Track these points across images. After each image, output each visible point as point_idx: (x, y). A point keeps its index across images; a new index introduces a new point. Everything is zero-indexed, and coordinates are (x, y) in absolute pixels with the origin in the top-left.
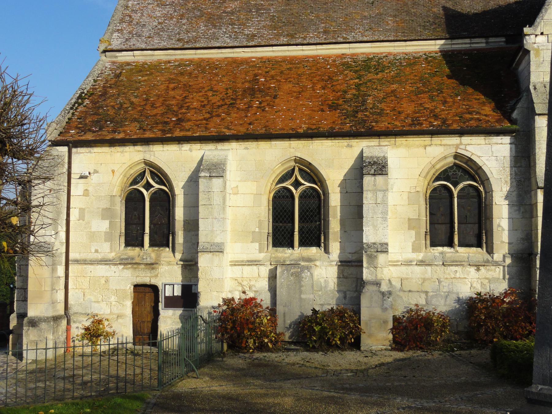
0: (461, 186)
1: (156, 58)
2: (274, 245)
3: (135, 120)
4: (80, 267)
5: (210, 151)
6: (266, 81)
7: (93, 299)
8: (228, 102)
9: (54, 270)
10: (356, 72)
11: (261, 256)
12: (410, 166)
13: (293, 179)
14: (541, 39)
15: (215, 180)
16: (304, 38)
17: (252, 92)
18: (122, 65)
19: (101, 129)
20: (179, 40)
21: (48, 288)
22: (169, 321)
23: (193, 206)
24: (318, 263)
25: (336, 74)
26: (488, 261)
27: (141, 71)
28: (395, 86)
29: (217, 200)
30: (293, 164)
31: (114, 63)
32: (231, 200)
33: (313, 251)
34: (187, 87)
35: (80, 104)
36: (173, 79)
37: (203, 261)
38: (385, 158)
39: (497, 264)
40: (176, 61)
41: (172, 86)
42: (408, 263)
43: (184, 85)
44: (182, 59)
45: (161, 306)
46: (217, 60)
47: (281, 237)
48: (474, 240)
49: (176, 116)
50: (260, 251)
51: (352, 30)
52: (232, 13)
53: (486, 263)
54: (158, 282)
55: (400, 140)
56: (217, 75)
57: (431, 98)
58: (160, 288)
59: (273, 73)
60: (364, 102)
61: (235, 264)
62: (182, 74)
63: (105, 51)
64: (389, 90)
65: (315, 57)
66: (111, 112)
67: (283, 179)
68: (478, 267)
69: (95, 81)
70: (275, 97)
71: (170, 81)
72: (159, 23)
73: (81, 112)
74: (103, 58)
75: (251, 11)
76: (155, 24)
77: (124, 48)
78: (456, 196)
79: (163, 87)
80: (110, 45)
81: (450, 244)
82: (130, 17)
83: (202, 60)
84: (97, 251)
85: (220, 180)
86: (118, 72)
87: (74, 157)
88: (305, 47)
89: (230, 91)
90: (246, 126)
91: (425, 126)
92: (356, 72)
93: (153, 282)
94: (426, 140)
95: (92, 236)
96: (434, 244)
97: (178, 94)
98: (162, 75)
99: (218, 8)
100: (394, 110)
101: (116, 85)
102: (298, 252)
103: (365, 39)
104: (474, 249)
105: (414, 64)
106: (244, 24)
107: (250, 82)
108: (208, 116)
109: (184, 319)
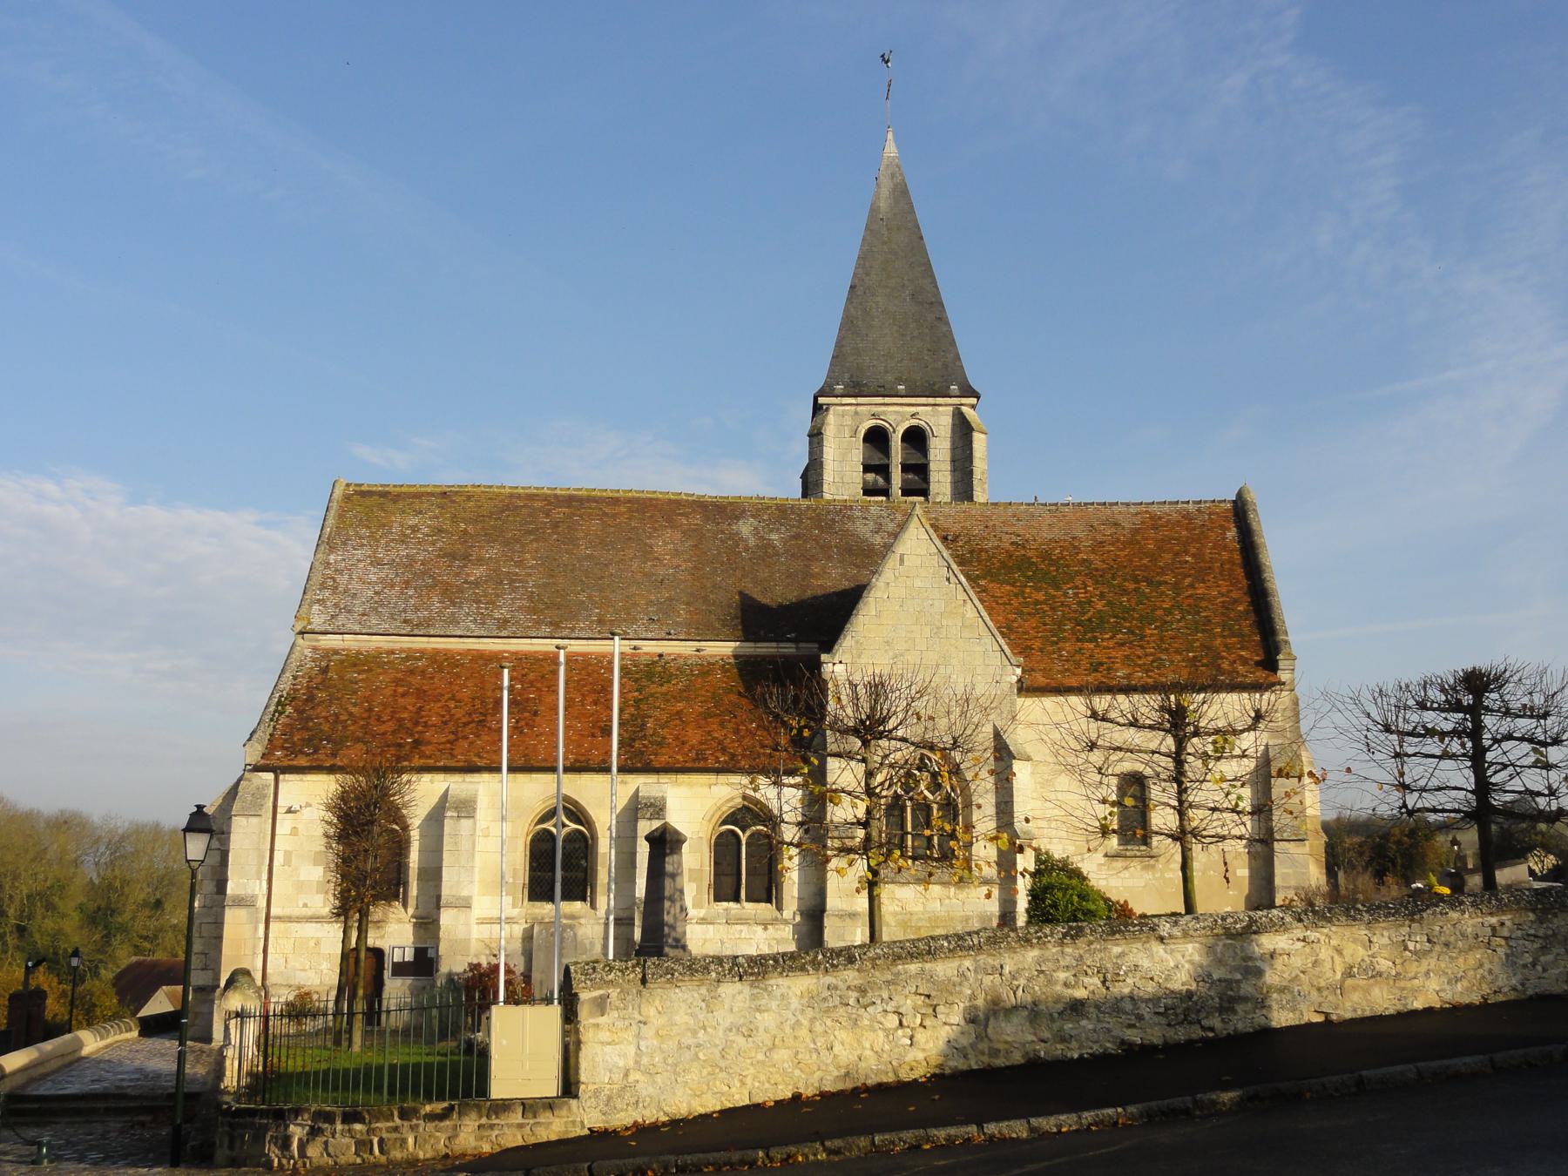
0: (748, 833)
1: (373, 645)
2: (530, 899)
3: (358, 740)
4: (282, 926)
5: (457, 784)
6: (523, 689)
7: (298, 966)
8: (476, 717)
10: (636, 681)
11: (515, 912)
12: (695, 805)
14: (839, 668)
15: (463, 821)
16: (573, 629)
18: (329, 653)
19: (316, 752)
20: (405, 621)
22: (396, 990)
23: (434, 850)
28: (680, 706)
29: (465, 845)
31: (315, 649)
32: (481, 844)
33: (577, 906)
34: (420, 693)
35: (281, 713)
37: (446, 918)
38: (664, 799)
39: (786, 922)
40: (402, 651)
41: (401, 690)
45: (387, 974)
47: (539, 889)
48: (764, 896)
49: (412, 735)
50: (514, 906)
51: (634, 621)
52: (477, 584)
53: (774, 921)
55: (682, 778)
56: (458, 676)
57: (722, 725)
59: (531, 676)
60: (643, 727)
61: (482, 922)
62: (412, 672)
63: (302, 633)
64: (675, 709)
66: (326, 727)
67: (543, 820)
68: (765, 926)
69: (295, 678)
70: (535, 714)
71: (397, 682)
73: (285, 725)
74: (300, 641)
76: (370, 593)
77: (330, 629)
79: (388, 692)
81: (737, 899)
82: (334, 580)
83: (437, 652)
84: (305, 905)
85: (471, 821)
86: (324, 664)
89: (477, 702)
91: (710, 763)
92: (636, 681)
94: (712, 778)
95: (300, 887)
96: (718, 898)
97: (409, 702)
98: (385, 672)
100: (677, 738)
101: (325, 684)
103: (650, 635)
105: (707, 673)
106: (493, 603)
108: (451, 737)
109: (415, 992)
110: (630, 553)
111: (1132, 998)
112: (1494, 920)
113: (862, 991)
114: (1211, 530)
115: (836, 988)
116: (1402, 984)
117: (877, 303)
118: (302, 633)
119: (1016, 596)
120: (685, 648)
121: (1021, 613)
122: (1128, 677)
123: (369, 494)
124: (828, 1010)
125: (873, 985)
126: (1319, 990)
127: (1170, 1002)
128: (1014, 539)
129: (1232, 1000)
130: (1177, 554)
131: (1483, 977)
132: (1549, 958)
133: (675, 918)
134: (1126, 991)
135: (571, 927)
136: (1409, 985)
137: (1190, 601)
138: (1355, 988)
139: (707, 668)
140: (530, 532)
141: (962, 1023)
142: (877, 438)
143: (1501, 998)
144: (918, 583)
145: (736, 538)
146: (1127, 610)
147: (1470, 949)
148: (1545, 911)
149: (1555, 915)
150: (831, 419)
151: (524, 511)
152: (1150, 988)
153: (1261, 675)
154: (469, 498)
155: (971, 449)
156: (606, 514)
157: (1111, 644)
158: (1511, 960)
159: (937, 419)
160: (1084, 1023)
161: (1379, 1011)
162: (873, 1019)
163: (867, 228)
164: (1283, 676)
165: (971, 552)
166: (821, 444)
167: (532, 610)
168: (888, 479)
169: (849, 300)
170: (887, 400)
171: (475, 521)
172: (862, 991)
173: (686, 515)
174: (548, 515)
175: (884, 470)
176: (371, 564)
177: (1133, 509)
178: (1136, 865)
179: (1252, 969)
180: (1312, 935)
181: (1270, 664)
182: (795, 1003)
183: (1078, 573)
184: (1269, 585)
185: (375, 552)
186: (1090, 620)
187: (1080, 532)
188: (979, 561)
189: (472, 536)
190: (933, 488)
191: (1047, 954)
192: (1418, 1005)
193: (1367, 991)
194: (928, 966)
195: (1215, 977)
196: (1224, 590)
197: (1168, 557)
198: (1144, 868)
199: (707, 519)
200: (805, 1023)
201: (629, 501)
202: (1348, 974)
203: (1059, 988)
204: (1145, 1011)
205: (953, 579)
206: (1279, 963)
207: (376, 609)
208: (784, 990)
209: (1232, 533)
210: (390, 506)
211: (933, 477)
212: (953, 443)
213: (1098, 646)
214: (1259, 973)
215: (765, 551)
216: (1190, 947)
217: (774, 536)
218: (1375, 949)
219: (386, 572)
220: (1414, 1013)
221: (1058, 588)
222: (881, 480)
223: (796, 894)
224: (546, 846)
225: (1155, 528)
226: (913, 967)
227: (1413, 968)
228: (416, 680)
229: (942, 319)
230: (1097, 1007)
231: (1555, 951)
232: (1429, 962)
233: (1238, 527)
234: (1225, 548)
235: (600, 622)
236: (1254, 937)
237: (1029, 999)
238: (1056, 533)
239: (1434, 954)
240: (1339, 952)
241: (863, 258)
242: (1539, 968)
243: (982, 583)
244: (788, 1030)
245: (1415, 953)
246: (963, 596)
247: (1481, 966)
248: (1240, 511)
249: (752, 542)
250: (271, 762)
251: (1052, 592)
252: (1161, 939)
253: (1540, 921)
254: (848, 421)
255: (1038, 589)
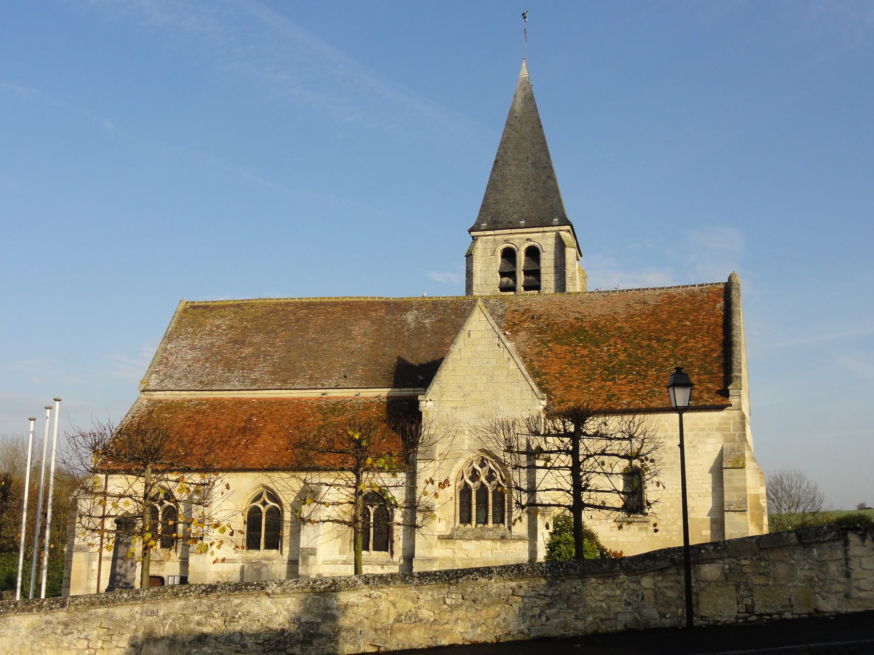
1: (181, 397)
9: (90, 565)
11: (236, 556)
12: (336, 492)
13: (262, 500)
14: (429, 404)
16: (293, 384)
17: (243, 431)
20: (201, 382)
21: (85, 578)
24: (275, 562)
25: (309, 415)
26: (389, 562)
27: (168, 409)
30: (262, 488)
31: (150, 400)
33: (274, 552)
34: (199, 424)
36: (190, 417)
39: (395, 564)
40: (196, 400)
41: (188, 423)
42: (335, 563)
43: (198, 423)
44: (201, 399)
46: (228, 400)
47: (252, 543)
52: (245, 358)
53: (388, 563)
54: (164, 574)
56: (223, 414)
58: (165, 578)
59: (264, 413)
62: (198, 412)
63: (143, 391)
65: (299, 399)
67: (255, 500)
69: (133, 417)
70: (258, 436)
71: (188, 418)
72: (189, 366)
74: (143, 396)
75: (259, 357)
77: (158, 388)
78: (372, 514)
80: (148, 385)
81: (258, 548)
82: (167, 359)
83: (216, 399)
87: (109, 482)
88: (293, 391)
90: (231, 460)
93: (161, 574)
97: (190, 431)
99: (236, 353)
102: (262, 553)
104: (383, 552)
105: (367, 408)
107: (245, 421)
110: (337, 335)
111: (241, 633)
112: (514, 584)
113: (66, 625)
114: (707, 303)
115: (51, 623)
116: (436, 627)
117: (510, 170)
118: (143, 391)
119: (570, 352)
120: (349, 393)
121: (570, 364)
122: (629, 404)
123: (199, 307)
124: (43, 637)
125: (74, 621)
126: (376, 630)
127: (267, 636)
128: (577, 315)
129: (312, 636)
130: (680, 321)
131: (498, 624)
132: (553, 611)
133: (126, 570)
134: (238, 628)
135: (266, 565)
136: (441, 628)
137: (683, 352)
138: (400, 630)
139: (368, 405)
140: (281, 326)
141: (127, 647)
142: (509, 255)
143: (510, 638)
144: (479, 348)
145: (403, 323)
146: (639, 359)
147: (492, 604)
148: (555, 578)
149: (563, 581)
150: (479, 244)
151: (282, 313)
152: (255, 627)
153: (718, 400)
154: (252, 307)
155: (564, 258)
156: (328, 312)
157: (624, 382)
158: (523, 614)
159: (545, 239)
160: (205, 649)
161: (415, 646)
162: (70, 643)
163: (507, 124)
164: (733, 400)
165: (548, 325)
166: (472, 262)
167: (273, 373)
168: (515, 281)
169: (493, 170)
170: (513, 231)
171: (253, 320)
172: (66, 625)
173: (375, 311)
174: (295, 314)
175: (512, 275)
176: (190, 349)
177: (657, 292)
178: (634, 527)
179: (329, 616)
180: (375, 593)
181: (725, 393)
182: (23, 632)
183: (613, 336)
184: (735, 339)
185: (194, 341)
186: (613, 367)
187: (620, 309)
188: (552, 331)
189: (249, 329)
190: (543, 284)
191: (190, 603)
192: (445, 642)
193: (408, 632)
194: (111, 610)
195: (303, 620)
196: (712, 344)
197: (674, 323)
198: (640, 529)
199: (388, 312)
200: (28, 644)
201: (344, 303)
202: (398, 620)
203: (192, 626)
204: (249, 642)
205: (502, 345)
206: (350, 613)
207: (186, 375)
208: (16, 623)
209: (720, 305)
210: (208, 314)
211: (543, 277)
212: (556, 256)
213: (615, 383)
214: (334, 618)
215: (421, 329)
216: (289, 600)
217: (427, 321)
218: (421, 602)
219: (198, 353)
220: (442, 647)
221: (598, 346)
222: (511, 281)
223: (401, 546)
224: (256, 515)
225: (670, 304)
226: (101, 611)
227: (447, 616)
228: (198, 417)
229: (551, 177)
230: (216, 638)
231: (559, 606)
232: (461, 613)
233: (725, 301)
234: (713, 315)
235: (311, 379)
236: (333, 594)
237: (172, 632)
238: (605, 311)
239: (464, 607)
240: (394, 604)
241: (503, 143)
242: (544, 618)
243: (550, 345)
244: (17, 649)
245: (450, 606)
246: (507, 355)
247: (499, 615)
248: (728, 290)
249: (412, 326)
250: (105, 468)
251: (594, 349)
252: (268, 594)
253: (550, 585)
254: (490, 245)
255: (584, 347)
